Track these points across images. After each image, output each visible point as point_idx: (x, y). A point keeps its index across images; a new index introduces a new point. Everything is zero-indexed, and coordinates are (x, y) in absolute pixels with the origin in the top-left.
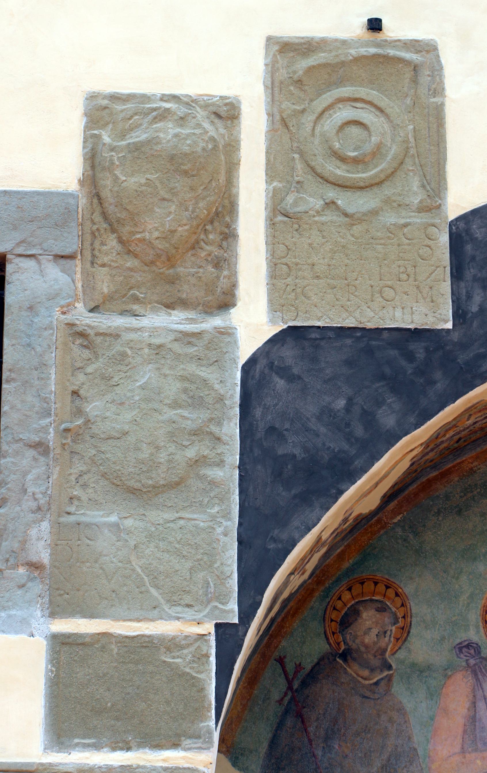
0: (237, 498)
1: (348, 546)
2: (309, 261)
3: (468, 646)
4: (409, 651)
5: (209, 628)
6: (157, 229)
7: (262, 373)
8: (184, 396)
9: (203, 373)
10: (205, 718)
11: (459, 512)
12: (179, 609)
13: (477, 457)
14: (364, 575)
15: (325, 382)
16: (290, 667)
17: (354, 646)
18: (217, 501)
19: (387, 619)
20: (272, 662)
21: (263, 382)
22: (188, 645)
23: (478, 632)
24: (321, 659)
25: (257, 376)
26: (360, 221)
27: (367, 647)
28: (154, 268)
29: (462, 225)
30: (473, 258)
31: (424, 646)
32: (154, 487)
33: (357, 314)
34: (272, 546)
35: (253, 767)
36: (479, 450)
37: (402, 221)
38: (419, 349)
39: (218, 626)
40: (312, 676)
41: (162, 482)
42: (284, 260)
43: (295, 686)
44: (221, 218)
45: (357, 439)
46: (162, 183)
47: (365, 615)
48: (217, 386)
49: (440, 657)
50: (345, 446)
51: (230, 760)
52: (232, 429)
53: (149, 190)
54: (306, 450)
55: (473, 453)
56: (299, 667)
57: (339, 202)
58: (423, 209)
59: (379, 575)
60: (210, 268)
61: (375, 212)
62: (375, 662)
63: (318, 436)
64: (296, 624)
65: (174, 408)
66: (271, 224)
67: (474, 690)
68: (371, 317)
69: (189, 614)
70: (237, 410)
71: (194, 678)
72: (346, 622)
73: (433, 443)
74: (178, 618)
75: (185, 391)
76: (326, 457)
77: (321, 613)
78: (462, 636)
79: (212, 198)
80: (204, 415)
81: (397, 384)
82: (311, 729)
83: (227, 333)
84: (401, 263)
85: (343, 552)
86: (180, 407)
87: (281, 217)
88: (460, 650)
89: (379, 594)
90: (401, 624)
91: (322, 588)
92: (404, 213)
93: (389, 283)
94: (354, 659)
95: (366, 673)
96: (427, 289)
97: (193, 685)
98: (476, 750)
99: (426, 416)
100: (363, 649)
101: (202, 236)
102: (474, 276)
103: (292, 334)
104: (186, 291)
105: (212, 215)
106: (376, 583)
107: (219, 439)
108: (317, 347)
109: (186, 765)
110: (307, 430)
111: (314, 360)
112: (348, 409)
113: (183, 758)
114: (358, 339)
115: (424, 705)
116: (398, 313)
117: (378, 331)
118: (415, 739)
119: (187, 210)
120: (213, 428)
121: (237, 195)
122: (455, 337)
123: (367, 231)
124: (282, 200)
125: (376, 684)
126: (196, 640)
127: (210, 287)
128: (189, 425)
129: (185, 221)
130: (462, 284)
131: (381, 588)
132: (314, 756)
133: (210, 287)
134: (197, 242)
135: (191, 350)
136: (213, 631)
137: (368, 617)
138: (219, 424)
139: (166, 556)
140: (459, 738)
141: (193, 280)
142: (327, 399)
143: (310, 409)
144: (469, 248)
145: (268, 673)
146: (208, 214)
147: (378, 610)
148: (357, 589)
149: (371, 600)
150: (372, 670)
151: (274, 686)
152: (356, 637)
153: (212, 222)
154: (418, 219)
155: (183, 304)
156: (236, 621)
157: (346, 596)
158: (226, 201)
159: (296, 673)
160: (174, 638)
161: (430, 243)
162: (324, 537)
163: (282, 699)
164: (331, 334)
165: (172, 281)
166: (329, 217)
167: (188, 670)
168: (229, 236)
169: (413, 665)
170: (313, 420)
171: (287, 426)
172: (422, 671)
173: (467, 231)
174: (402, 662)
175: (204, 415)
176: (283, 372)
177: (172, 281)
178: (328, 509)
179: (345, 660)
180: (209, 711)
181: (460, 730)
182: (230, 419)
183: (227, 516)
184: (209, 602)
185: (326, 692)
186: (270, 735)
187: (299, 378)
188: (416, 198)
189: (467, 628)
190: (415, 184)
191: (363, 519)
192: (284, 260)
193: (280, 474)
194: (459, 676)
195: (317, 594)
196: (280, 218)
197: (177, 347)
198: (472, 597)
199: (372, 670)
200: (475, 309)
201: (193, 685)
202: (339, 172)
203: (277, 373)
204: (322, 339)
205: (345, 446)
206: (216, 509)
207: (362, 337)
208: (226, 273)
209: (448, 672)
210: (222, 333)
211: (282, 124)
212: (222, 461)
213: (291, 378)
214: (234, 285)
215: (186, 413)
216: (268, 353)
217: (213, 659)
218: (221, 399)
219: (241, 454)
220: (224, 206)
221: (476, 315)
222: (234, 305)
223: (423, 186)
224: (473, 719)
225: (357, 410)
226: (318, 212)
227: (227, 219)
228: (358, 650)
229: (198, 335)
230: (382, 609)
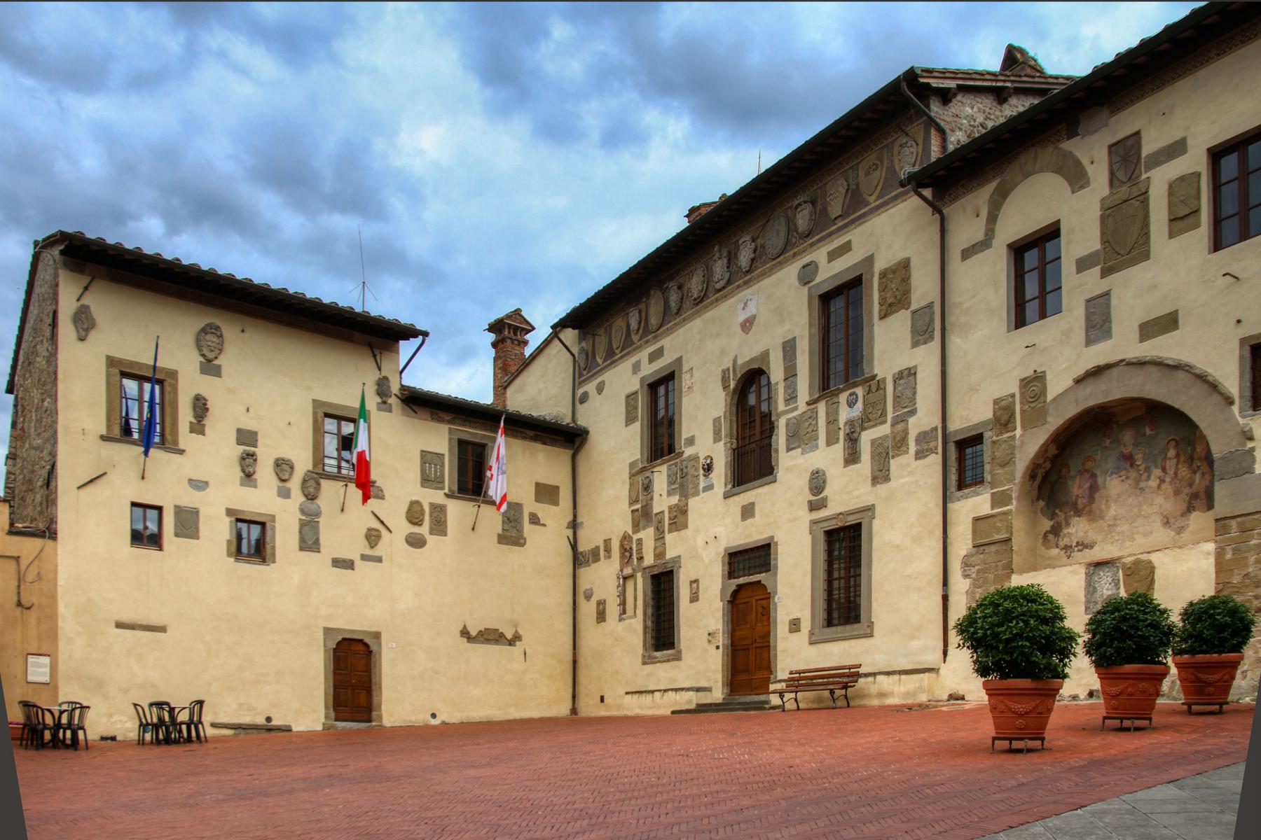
31: (1072, 473)
44: (1013, 415)
87: (1022, 411)
211: (1022, 394)
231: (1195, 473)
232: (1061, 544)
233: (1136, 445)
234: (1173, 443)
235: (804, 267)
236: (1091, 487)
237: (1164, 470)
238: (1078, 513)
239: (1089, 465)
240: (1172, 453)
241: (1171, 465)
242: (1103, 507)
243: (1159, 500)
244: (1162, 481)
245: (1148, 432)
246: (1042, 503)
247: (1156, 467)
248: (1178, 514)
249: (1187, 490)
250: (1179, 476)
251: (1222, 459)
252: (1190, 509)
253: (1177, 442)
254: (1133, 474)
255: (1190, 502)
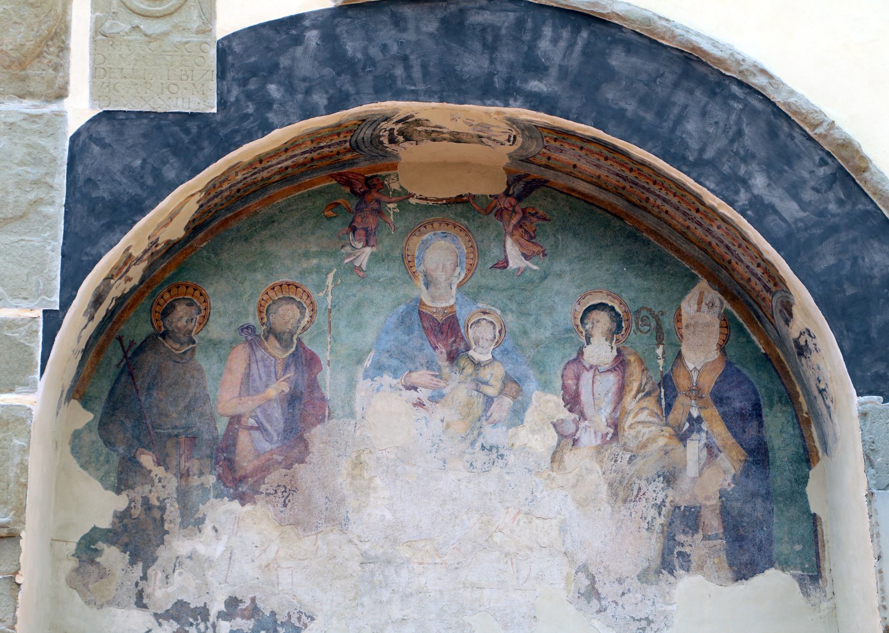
0: (63, 226)
1: (170, 263)
2: (120, 67)
3: (247, 328)
4: (208, 332)
5: (39, 313)
6: (11, 43)
7: (84, 142)
8: (28, 158)
9: (43, 142)
10: (34, 373)
11: (246, 240)
12: (18, 300)
13: (259, 204)
14: (180, 282)
15: (128, 148)
16: (126, 343)
17: (170, 329)
18: (48, 228)
19: (194, 310)
20: (114, 340)
21: (84, 148)
22: (24, 325)
23: (254, 319)
24: (148, 337)
25: (80, 144)
26: (156, 39)
27: (179, 329)
28: (10, 70)
29: (226, 43)
30: (233, 65)
31: (218, 328)
32: (4, 219)
33: (151, 103)
34: (85, 258)
35: (97, 408)
36: (260, 198)
37: (185, 40)
38: (193, 126)
39: (45, 312)
40: (141, 349)
41: (10, 216)
42: (102, 66)
43: (129, 355)
44: (58, 37)
45: (148, 187)
46: (15, 11)
47: (179, 308)
48: (52, 151)
49: (228, 335)
50: (139, 191)
51: (82, 404)
52: (61, 180)
53: (5, 16)
54: (112, 194)
55: (257, 201)
56: (132, 343)
57: (142, 27)
58: (199, 32)
59: (190, 282)
60: (51, 71)
61: (166, 34)
62: (184, 339)
63: (121, 184)
64: (132, 314)
65: (21, 166)
66: (94, 41)
67: (249, 357)
68: (161, 106)
69: (25, 303)
70: (65, 167)
71: (26, 346)
72: (166, 312)
73: (211, 189)
74: (17, 307)
75: (30, 154)
76: (126, 199)
77: (149, 307)
78: (244, 321)
79: (51, 23)
80: (42, 170)
81: (177, 150)
82: (138, 383)
83: (60, 115)
84: (183, 68)
85: (166, 267)
86: (25, 165)
87: (100, 35)
88: (242, 330)
89: (189, 294)
90: (203, 314)
91: (150, 291)
92: (186, 34)
93: (174, 82)
94: (170, 337)
95: (178, 346)
96: (200, 85)
97: (26, 351)
98: (249, 395)
99: (196, 171)
100: (176, 330)
101: (45, 49)
102: (233, 77)
103: (107, 115)
104: (33, 86)
105: (52, 34)
106: (187, 287)
107: (52, 187)
108: (123, 124)
109: (17, 404)
110: (114, 180)
111: (121, 133)
112: (142, 167)
113: (16, 399)
114: (152, 119)
115: (215, 366)
116: (180, 102)
117: (166, 114)
118: (208, 388)
119: (33, 30)
120: (48, 179)
121: (70, 21)
122: (219, 118)
123: (160, 46)
124: (102, 25)
125: (184, 353)
126: (30, 321)
127: (50, 84)
128: (31, 177)
129: (31, 38)
130: (225, 83)
131: (191, 290)
132: (139, 400)
133: (50, 84)
134: (41, 53)
135: (35, 127)
136: (41, 315)
137: (181, 310)
138: (53, 176)
139: (11, 264)
140: (238, 389)
141: (38, 79)
142: (129, 160)
143: (116, 166)
144: (230, 58)
145: (111, 347)
146: (49, 34)
147: (188, 305)
148: (174, 291)
149: (184, 298)
150: (182, 344)
151: (114, 355)
152: (172, 323)
153: (52, 39)
154: (196, 39)
155: (31, 95)
156: (58, 308)
157: (167, 296)
158: (63, 25)
159: (130, 346)
160: (13, 320)
161: (203, 54)
162: (136, 253)
163: (119, 364)
164: (133, 116)
165: (23, 79)
166: (134, 36)
167: (22, 341)
168: (64, 49)
169: (210, 340)
170: (118, 174)
171: (100, 178)
172: (215, 344)
173: (229, 47)
174: (203, 339)
175: (42, 170)
176: (99, 142)
177: (23, 79)
178: (125, 233)
179: (164, 338)
180: (36, 368)
181: (239, 381)
182: (60, 174)
183: (55, 238)
184: (39, 296)
185: (150, 359)
186: (110, 387)
187: (110, 145)
188: (195, 24)
189: (247, 316)
190: (195, 14)
191: (174, 244)
192: (102, 66)
193: (93, 210)
194: (240, 347)
195: (147, 295)
196: (100, 37)
197: (25, 125)
198: (251, 295)
199: (182, 344)
200: (232, 99)
201: (26, 351)
202: (142, 6)
203: (95, 143)
204: (127, 119)
205: (139, 191)
206: (48, 234)
207: (155, 118)
208: (61, 74)
209: (233, 344)
210: (56, 115)
212: (54, 202)
213: (104, 146)
214: (67, 83)
215: (29, 169)
216: (88, 129)
217: (41, 334)
218: (54, 160)
219: (67, 197)
220: (61, 29)
221: (233, 104)
222: (67, 96)
223: (200, 16)
224: (248, 375)
225: (149, 167)
226: (127, 33)
227: (63, 37)
228: (173, 331)
229: (40, 116)
230: (191, 304)
231: (683, 439)
232: (162, 594)
233: (471, 291)
234: (602, 320)
235: (869, 462)
236: (293, 399)
237: (572, 401)
238: (238, 484)
239: (287, 315)
240: (600, 351)
241: (599, 391)
242: (342, 481)
243: (556, 502)
244: (568, 440)
245: (516, 260)
246: (84, 417)
247: (545, 386)
248: (629, 567)
249: (656, 491)
250: (628, 433)
251: (284, 68)
252: (670, 561)
253: (617, 318)
254: (458, 388)
255: (670, 538)
